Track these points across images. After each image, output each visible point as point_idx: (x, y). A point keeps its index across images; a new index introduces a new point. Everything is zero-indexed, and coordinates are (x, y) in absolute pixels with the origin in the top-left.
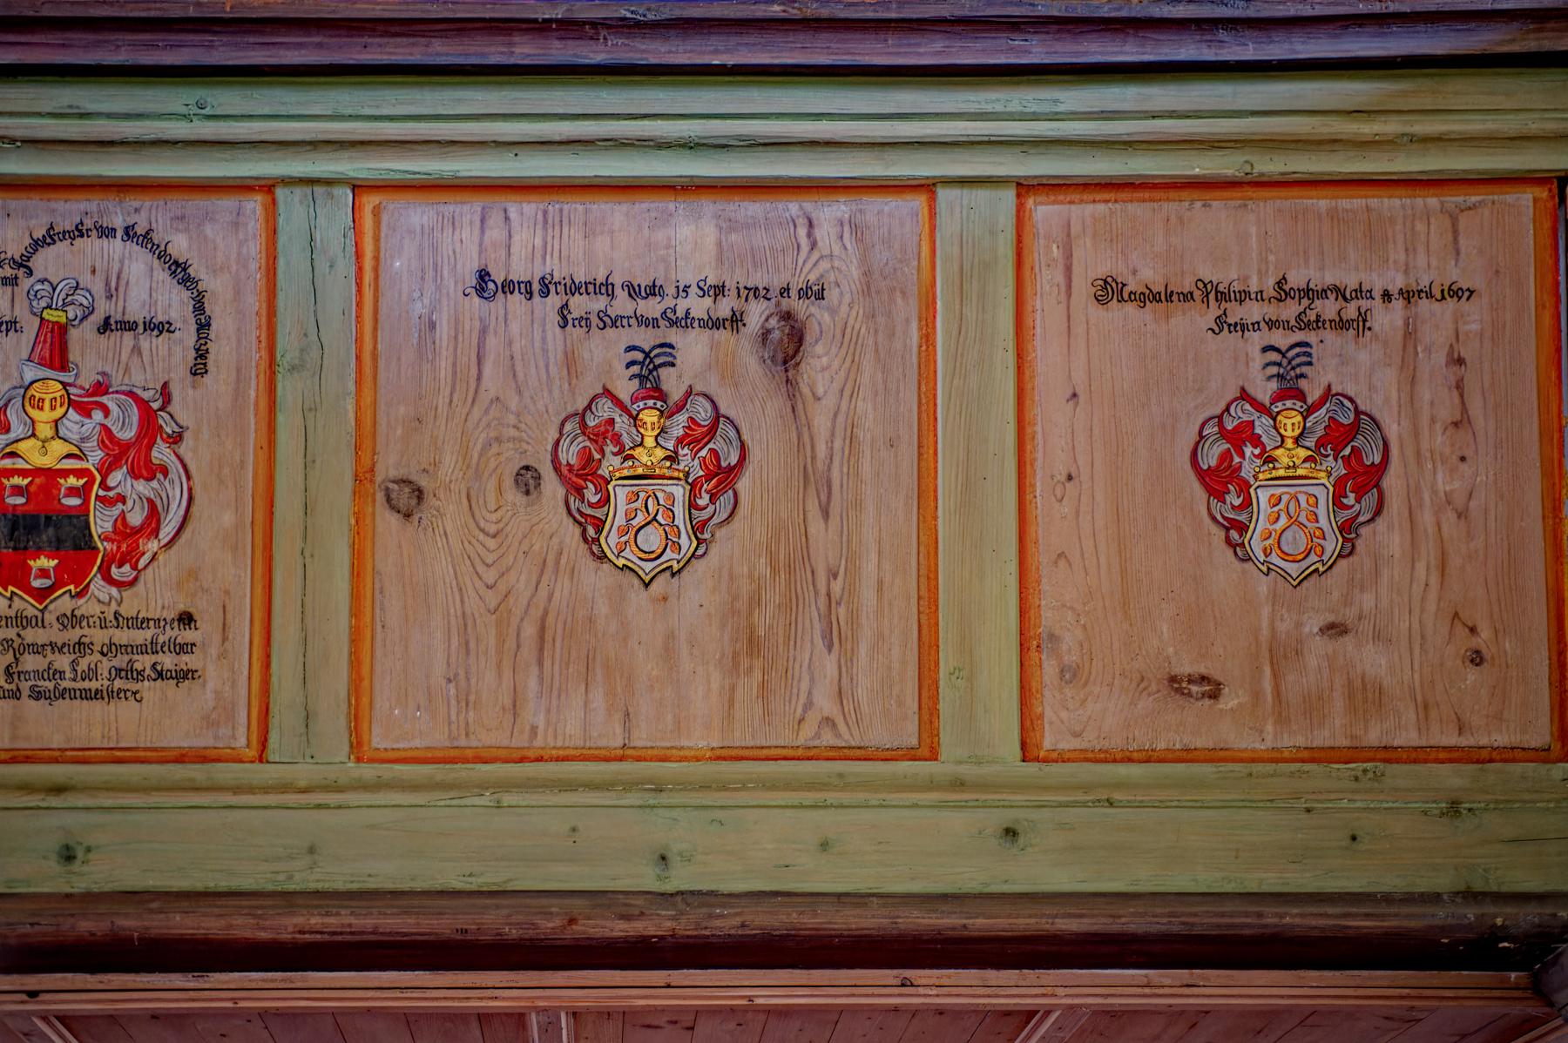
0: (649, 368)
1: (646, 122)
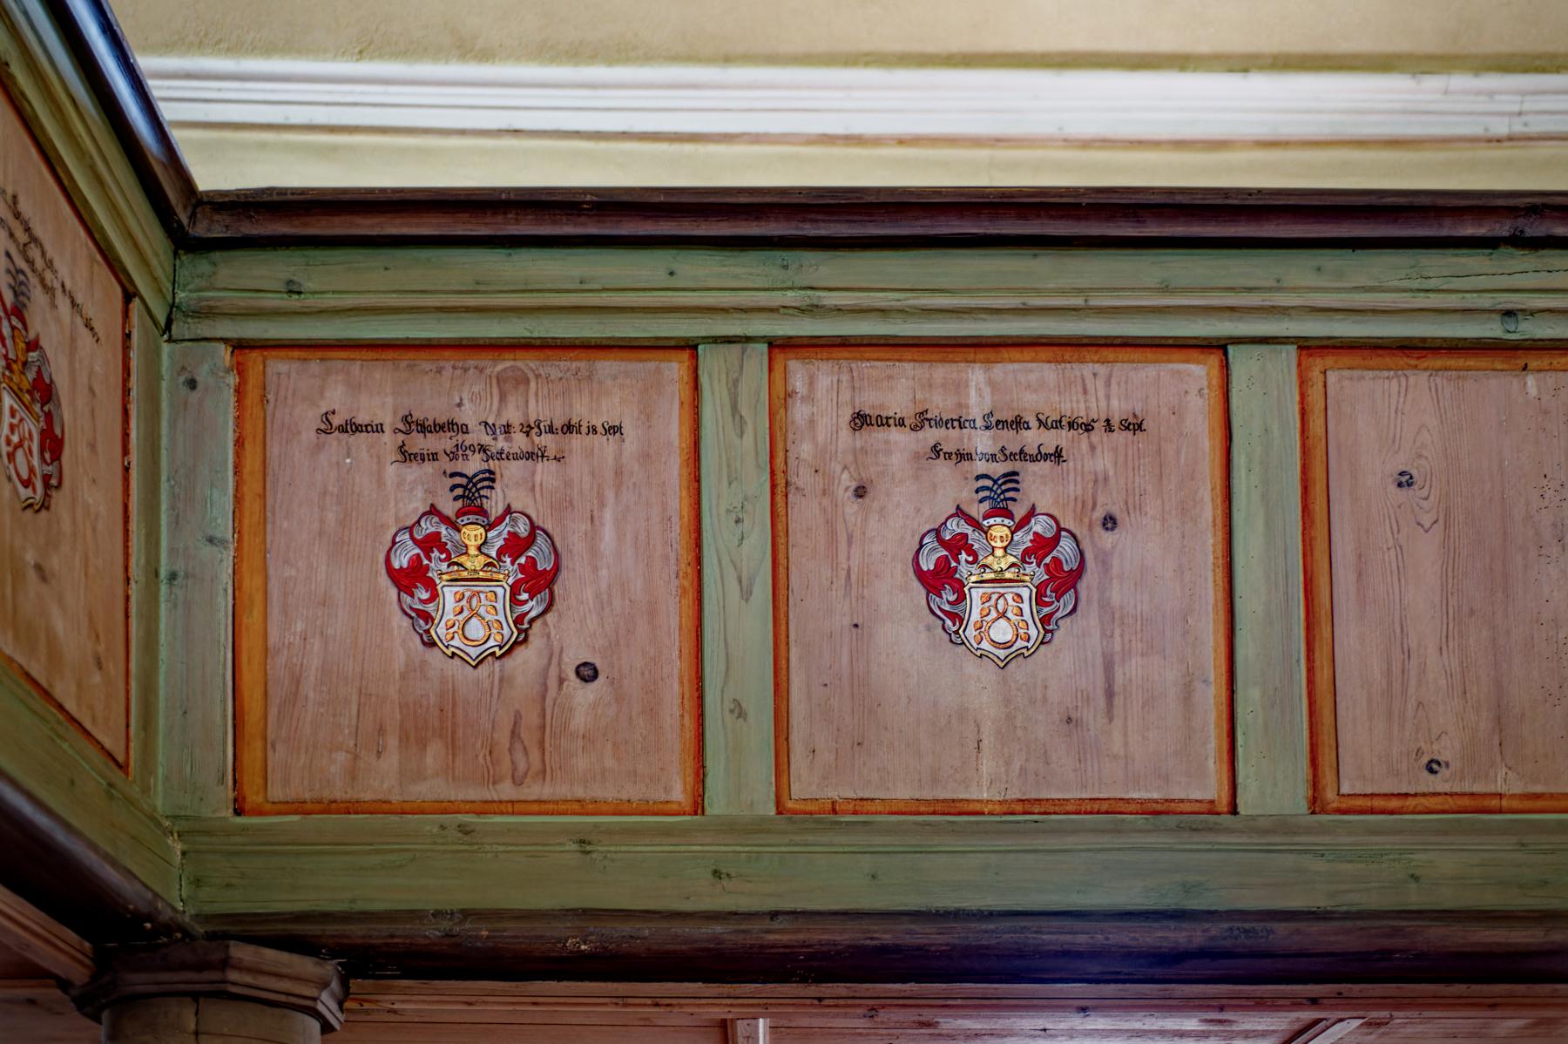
0: (471, 497)
1: (670, 293)
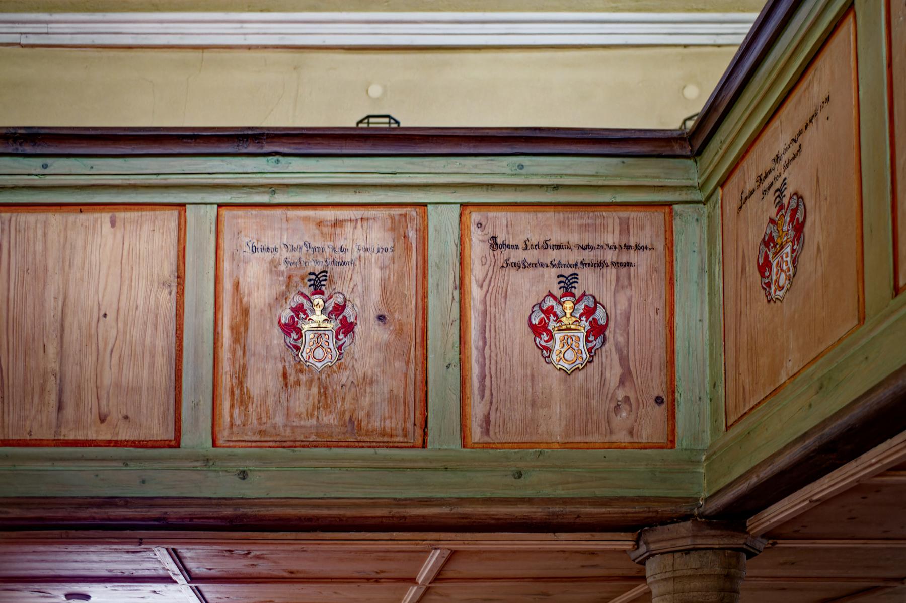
0: (568, 285)
